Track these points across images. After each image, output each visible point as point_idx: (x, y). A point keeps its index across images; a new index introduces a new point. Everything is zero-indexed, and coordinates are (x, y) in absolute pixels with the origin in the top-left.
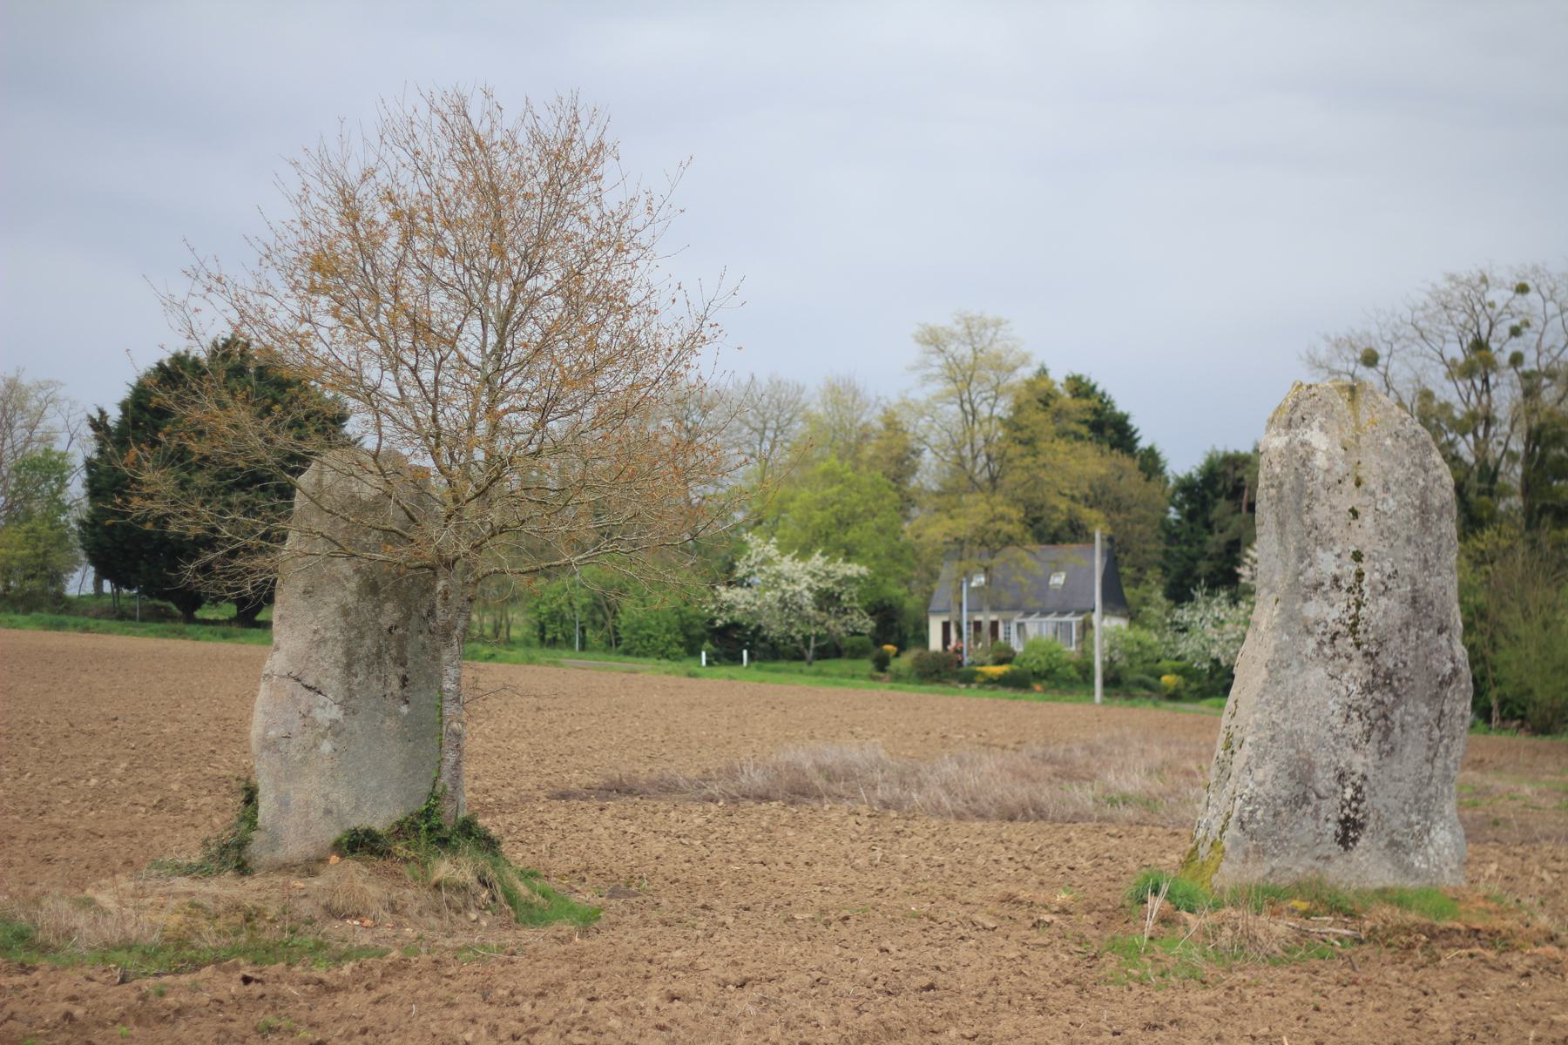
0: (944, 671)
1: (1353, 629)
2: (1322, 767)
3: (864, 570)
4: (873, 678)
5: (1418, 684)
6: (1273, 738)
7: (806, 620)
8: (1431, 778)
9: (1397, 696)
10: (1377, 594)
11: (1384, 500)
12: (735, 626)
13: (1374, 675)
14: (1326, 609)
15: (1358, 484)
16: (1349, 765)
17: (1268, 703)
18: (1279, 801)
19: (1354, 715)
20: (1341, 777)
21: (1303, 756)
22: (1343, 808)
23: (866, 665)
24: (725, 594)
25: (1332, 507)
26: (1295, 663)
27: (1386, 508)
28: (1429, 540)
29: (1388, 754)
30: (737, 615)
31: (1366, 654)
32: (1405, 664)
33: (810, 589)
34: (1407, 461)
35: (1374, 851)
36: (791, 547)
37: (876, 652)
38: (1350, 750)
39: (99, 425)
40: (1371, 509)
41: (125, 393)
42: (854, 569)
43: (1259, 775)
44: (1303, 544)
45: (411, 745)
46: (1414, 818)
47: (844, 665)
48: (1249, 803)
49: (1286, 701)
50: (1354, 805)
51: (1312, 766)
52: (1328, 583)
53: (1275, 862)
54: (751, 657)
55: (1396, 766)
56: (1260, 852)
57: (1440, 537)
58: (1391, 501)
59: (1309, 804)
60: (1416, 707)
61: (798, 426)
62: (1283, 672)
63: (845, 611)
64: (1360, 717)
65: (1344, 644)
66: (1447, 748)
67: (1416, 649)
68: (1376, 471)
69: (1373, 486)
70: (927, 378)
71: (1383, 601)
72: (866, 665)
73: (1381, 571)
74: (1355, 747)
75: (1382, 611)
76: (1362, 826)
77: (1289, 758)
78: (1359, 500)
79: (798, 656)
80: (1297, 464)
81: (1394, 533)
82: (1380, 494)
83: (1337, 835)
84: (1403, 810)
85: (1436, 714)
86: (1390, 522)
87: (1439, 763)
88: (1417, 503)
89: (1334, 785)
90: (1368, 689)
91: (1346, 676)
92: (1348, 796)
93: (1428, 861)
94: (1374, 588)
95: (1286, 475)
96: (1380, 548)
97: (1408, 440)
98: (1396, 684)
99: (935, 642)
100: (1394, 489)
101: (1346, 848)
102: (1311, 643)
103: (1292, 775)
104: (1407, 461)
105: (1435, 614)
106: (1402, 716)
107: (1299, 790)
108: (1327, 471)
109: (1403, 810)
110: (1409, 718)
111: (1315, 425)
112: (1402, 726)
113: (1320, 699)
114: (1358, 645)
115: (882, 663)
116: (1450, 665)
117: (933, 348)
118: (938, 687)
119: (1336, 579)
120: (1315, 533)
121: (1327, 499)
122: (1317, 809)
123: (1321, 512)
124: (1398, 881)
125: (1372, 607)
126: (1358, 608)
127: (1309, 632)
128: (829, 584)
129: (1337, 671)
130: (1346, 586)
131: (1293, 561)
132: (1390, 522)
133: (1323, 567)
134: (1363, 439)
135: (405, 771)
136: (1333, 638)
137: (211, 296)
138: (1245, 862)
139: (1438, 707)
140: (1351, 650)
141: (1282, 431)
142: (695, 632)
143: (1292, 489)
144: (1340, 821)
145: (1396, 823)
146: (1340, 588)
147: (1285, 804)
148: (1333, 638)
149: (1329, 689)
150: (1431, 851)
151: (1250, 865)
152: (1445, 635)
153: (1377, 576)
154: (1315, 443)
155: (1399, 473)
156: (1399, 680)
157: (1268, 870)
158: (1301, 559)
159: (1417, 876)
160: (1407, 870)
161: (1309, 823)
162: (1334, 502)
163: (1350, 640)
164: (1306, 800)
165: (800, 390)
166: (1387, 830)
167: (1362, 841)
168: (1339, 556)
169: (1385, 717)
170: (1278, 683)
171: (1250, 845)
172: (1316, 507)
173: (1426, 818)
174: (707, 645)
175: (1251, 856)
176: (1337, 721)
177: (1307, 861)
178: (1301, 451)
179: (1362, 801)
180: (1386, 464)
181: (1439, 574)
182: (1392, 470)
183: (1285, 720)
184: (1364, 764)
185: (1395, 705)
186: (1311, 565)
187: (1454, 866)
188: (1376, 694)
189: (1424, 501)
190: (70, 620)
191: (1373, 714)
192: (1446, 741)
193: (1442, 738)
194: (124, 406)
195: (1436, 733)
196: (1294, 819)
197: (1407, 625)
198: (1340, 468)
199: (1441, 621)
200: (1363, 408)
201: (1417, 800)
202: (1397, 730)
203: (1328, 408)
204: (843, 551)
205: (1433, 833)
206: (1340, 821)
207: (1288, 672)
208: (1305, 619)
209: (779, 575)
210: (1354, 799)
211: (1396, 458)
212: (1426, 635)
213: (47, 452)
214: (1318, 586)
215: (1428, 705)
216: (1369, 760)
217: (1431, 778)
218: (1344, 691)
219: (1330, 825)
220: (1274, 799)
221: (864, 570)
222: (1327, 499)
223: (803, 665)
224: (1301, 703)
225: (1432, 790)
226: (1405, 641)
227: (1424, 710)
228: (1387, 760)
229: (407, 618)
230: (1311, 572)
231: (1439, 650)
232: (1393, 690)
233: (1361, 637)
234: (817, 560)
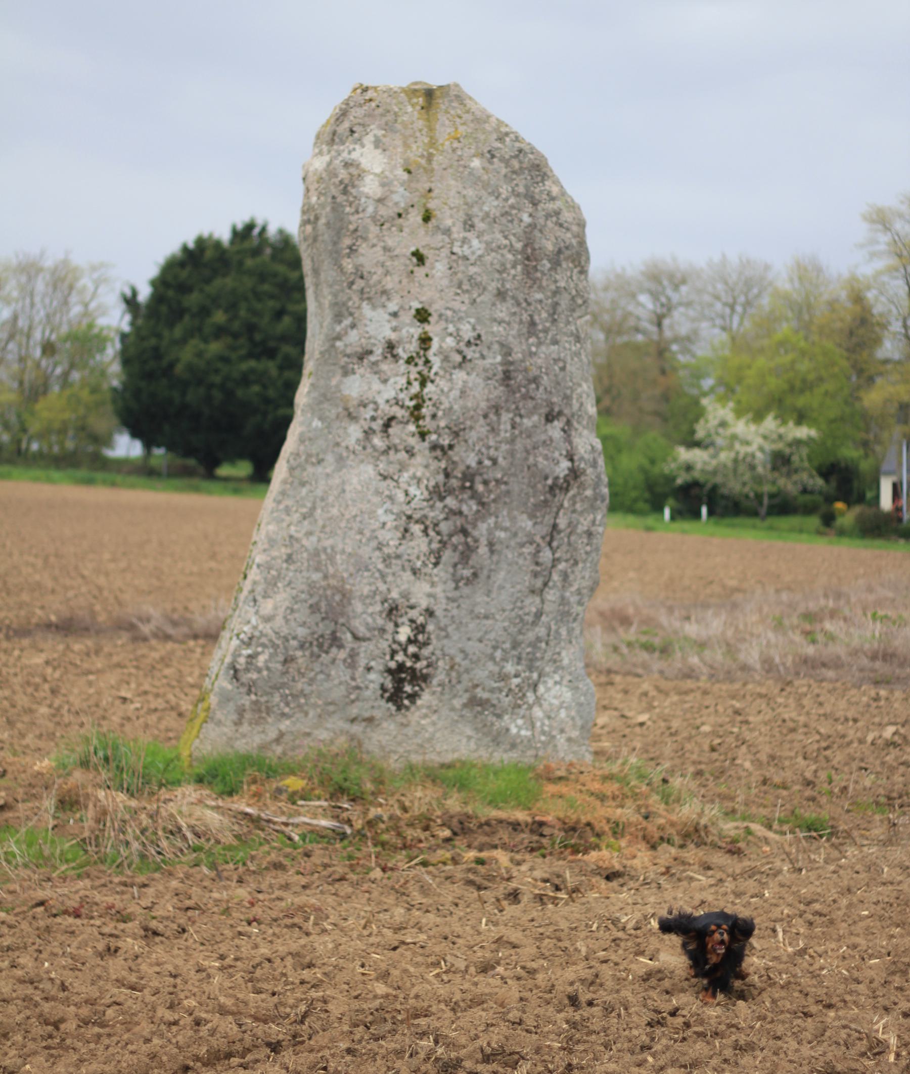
0: (881, 528)
1: (416, 413)
2: (363, 598)
3: (813, 433)
4: (819, 533)
5: (515, 487)
6: (289, 559)
7: (758, 480)
8: (539, 614)
9: (482, 504)
10: (450, 367)
11: (464, 241)
12: (696, 484)
13: (447, 475)
14: (376, 385)
15: (427, 218)
16: (406, 595)
17: (287, 511)
18: (294, 643)
19: (416, 529)
20: (392, 611)
21: (333, 582)
22: (393, 653)
23: (814, 521)
24: (684, 454)
25: (386, 249)
26: (330, 458)
27: (466, 251)
28: (539, 296)
29: (468, 582)
30: (696, 474)
31: (434, 447)
32: (494, 461)
33: (761, 449)
34: (505, 190)
35: (445, 712)
36: (747, 411)
37: (824, 508)
38: (408, 575)
39: (131, 302)
40: (445, 252)
41: (153, 271)
42: (803, 432)
43: (267, 607)
44: (342, 298)
46: (510, 668)
47: (794, 521)
48: (248, 644)
49: (313, 508)
50: (412, 649)
51: (346, 596)
52: (379, 351)
53: (285, 725)
54: (711, 513)
55: (480, 598)
56: (261, 711)
57: (556, 293)
58: (475, 243)
59: (341, 647)
60: (513, 519)
61: (766, 301)
62: (310, 469)
63: (796, 471)
64: (425, 531)
65: (405, 433)
66: (565, 576)
67: (512, 441)
68: (456, 201)
69: (449, 222)
70: (873, 255)
71: (460, 376)
72: (814, 521)
73: (457, 336)
74: (415, 572)
75: (458, 390)
76: (425, 678)
77: (312, 586)
78: (427, 240)
79: (754, 514)
80: (334, 191)
81: (478, 285)
82: (458, 233)
83: (383, 689)
84: (492, 658)
85: (545, 530)
86: (473, 270)
87: (551, 595)
88: (519, 246)
89: (380, 622)
90: (437, 494)
91: (406, 476)
92: (402, 637)
93: (533, 726)
94: (446, 359)
95: (323, 206)
96: (456, 305)
97: (507, 162)
98: (480, 488)
99: (886, 502)
100: (480, 226)
101: (399, 707)
102: (355, 432)
103: (314, 608)
104: (505, 190)
105: (540, 394)
106: (490, 532)
107: (325, 629)
108: (380, 201)
109: (492, 658)
110: (502, 535)
111: (369, 140)
112: (491, 544)
113: (365, 507)
114: (423, 435)
115: (828, 519)
116: (565, 464)
117: (880, 227)
118: (878, 542)
119: (391, 346)
120: (359, 284)
121: (380, 238)
122: (353, 655)
123: (369, 256)
124: (483, 753)
125: (443, 384)
126: (423, 384)
127: (352, 417)
128: (780, 446)
129: (392, 469)
130: (405, 356)
131: (328, 320)
132: (473, 270)
133: (371, 329)
134: (438, 159)
136: (387, 425)
138: (238, 723)
139: (549, 520)
140: (413, 441)
141: (325, 148)
142: (659, 489)
143: (328, 224)
144: (389, 671)
145: (480, 674)
146: (396, 357)
147: (302, 647)
148: (387, 425)
149: (378, 493)
150: (538, 712)
151: (245, 728)
152: (558, 424)
153: (450, 342)
154: (365, 163)
155: (491, 205)
156: (486, 483)
157: (273, 734)
158: (338, 318)
159: (513, 746)
160: (498, 738)
161: (340, 673)
162: (390, 243)
163: (412, 428)
164: (335, 641)
165: (767, 267)
166: (466, 683)
167: (426, 698)
168: (395, 315)
169: (464, 532)
170: (303, 484)
171: (246, 701)
172: (363, 248)
174: (671, 501)
175: (248, 716)
176: (390, 537)
177: (337, 723)
178: (343, 174)
179: (426, 644)
180: (470, 193)
181: (555, 342)
182: (479, 201)
183: (309, 534)
184: (430, 595)
185: (479, 516)
186: (353, 326)
187: (575, 734)
188: (450, 502)
189: (529, 243)
190: (99, 475)
191: (444, 527)
192: (562, 566)
193: (555, 561)
194: (154, 283)
195: (546, 555)
196: (317, 667)
197: (497, 409)
198: (400, 197)
199: (551, 404)
200: (443, 118)
201: (515, 645)
202: (483, 550)
203: (390, 117)
204: (795, 415)
205: (541, 689)
206: (389, 671)
207: (320, 469)
208: (345, 399)
209: (734, 437)
210: (410, 641)
211: (486, 185)
212: (527, 422)
213: (91, 326)
214: (364, 355)
215: (532, 516)
216: (438, 590)
217: (539, 614)
218: (401, 497)
219: (372, 676)
220: (286, 639)
221: (813, 433)
222: (380, 238)
223: (757, 521)
224: (335, 511)
225: (541, 631)
226: (493, 430)
228: (466, 591)
230: (353, 336)
231: (548, 443)
232: (475, 495)
233: (427, 423)
234: (770, 423)
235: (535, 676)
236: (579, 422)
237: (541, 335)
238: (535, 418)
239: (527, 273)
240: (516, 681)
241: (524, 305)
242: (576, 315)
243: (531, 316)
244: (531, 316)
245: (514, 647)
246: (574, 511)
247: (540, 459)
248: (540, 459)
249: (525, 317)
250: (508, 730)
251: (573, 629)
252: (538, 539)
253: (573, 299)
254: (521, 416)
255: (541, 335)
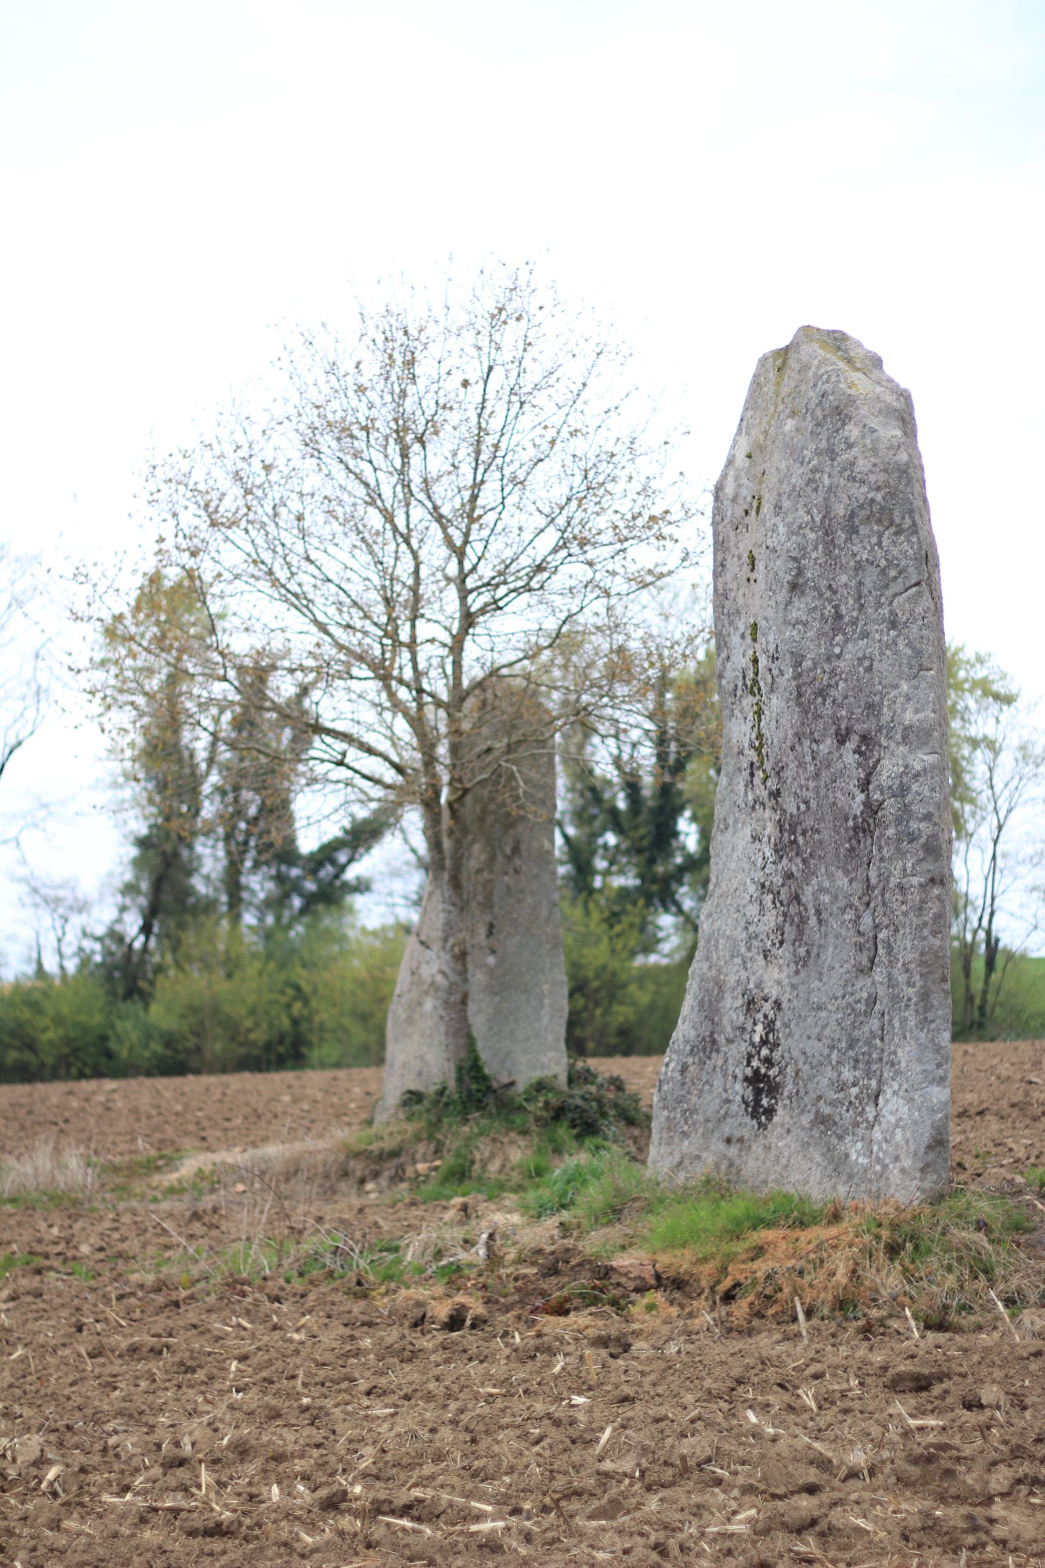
22: (750, 1057)
28: (844, 578)
45: (497, 999)
46: (848, 1074)
50: (765, 1052)
60: (831, 876)
66: (889, 948)
92: (757, 1039)
110: (826, 898)
112: (818, 913)
135: (491, 1028)
137: (357, 552)
160: (838, 1164)
173: (869, 1074)
181: (866, 635)
201: (852, 1044)
202: (813, 921)
210: (764, 1042)
212: (824, 748)
225: (875, 1024)
227: (843, 881)
229: (492, 858)
235: (874, 1083)
236: (889, 737)
237: (849, 629)
238: (829, 741)
239: (828, 553)
240: (854, 1091)
241: (828, 594)
242: (889, 593)
243: (836, 607)
244: (836, 607)
245: (851, 1047)
246: (882, 860)
247: (838, 795)
248: (838, 795)
249: (829, 610)
250: (847, 1156)
251: (906, 1019)
252: (856, 901)
253: (883, 572)
254: (816, 742)
255: (849, 629)
